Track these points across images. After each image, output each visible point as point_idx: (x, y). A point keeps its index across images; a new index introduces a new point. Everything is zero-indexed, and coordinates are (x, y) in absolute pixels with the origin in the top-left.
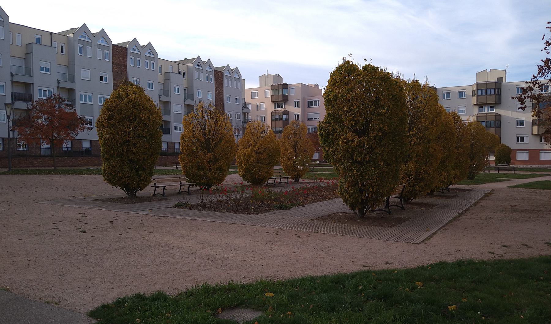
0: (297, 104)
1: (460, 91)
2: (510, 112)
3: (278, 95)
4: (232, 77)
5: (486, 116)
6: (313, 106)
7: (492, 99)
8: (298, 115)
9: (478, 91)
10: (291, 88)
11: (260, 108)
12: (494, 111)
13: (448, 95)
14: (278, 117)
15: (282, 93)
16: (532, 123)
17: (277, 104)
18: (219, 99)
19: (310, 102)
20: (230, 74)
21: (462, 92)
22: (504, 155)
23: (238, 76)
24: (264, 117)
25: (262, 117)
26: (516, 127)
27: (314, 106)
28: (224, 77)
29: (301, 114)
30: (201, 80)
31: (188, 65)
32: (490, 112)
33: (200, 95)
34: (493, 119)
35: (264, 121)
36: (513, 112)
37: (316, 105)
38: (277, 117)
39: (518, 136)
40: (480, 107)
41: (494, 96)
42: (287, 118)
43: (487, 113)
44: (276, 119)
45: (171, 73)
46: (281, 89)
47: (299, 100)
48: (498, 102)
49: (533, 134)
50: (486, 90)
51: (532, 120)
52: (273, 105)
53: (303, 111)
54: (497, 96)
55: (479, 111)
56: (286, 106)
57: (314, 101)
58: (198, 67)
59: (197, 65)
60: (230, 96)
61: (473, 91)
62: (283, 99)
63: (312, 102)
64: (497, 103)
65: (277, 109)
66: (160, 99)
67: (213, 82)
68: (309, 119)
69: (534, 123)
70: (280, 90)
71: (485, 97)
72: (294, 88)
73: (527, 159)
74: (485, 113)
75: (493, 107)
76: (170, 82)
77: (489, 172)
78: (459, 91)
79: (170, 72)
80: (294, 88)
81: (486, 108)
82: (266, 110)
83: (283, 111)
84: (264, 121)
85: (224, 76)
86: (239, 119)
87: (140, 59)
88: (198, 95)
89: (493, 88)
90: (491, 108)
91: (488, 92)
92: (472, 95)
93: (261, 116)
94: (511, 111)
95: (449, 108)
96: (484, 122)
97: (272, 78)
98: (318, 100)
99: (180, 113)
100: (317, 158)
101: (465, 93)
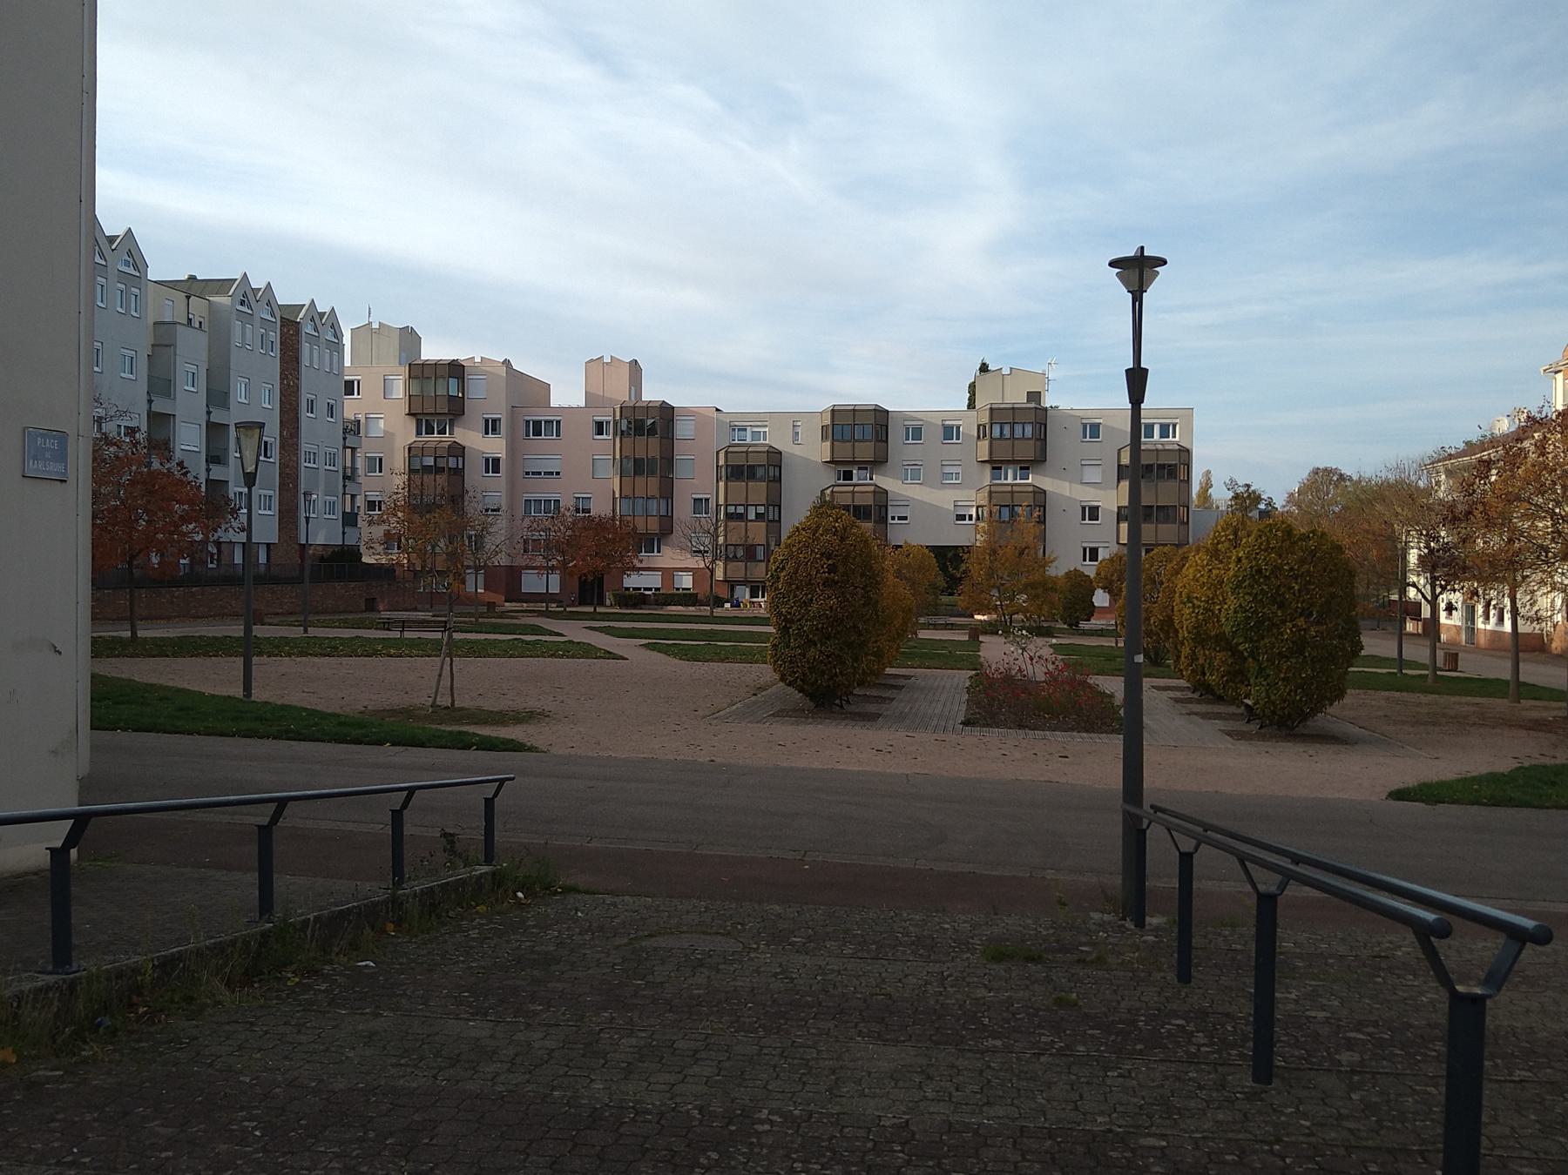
0: (491, 426)
1: (947, 423)
2: (1067, 484)
3: (433, 395)
4: (322, 340)
5: (1012, 492)
6: (541, 435)
7: (1026, 451)
8: (496, 461)
9: (994, 425)
10: (475, 377)
11: (367, 432)
12: (1030, 481)
13: (917, 433)
14: (432, 464)
15: (446, 390)
16: (1118, 514)
17: (427, 421)
18: (288, 407)
19: (531, 423)
20: (316, 329)
21: (951, 427)
22: (1080, 596)
23: (336, 336)
24: (381, 460)
25: (375, 458)
26: (1082, 524)
27: (543, 437)
28: (304, 339)
29: (504, 457)
30: (248, 347)
31: (211, 299)
32: (1018, 481)
33: (267, 401)
34: (1029, 501)
35: (380, 471)
36: (1073, 485)
37: (550, 434)
38: (430, 461)
39: (1085, 545)
40: (994, 468)
41: (1032, 442)
42: (460, 466)
43: (1012, 485)
44: (427, 469)
45: (178, 326)
46: (443, 377)
47: (500, 413)
48: (1038, 460)
49: (1121, 542)
50: (1012, 425)
51: (1118, 507)
52: (412, 425)
53: (512, 449)
54: (1038, 443)
55: (993, 478)
56: (456, 429)
57: (545, 422)
58: (240, 308)
59: (238, 302)
60: (334, 402)
61: (979, 426)
62: (449, 410)
63: (537, 424)
64: (1038, 461)
65: (425, 438)
66: (150, 408)
67: (277, 353)
68: (527, 473)
69: (1121, 516)
70: (440, 381)
71: (1009, 442)
72: (484, 377)
73: (1107, 605)
74: (1008, 485)
75: (1025, 467)
76: (175, 355)
77: (1117, 645)
78: (944, 422)
79: (175, 323)
80: (484, 377)
81: (1009, 471)
82: (388, 436)
83: (449, 446)
84: (380, 471)
85: (304, 334)
86: (315, 466)
87: (104, 280)
88: (239, 394)
89: (1029, 423)
90: (1023, 471)
91: (1018, 429)
92: (976, 435)
93: (367, 455)
94: (1070, 482)
95: (918, 467)
96: (1008, 508)
97: (396, 336)
98: (558, 418)
99: (196, 449)
100: (545, 591)
101: (958, 428)
